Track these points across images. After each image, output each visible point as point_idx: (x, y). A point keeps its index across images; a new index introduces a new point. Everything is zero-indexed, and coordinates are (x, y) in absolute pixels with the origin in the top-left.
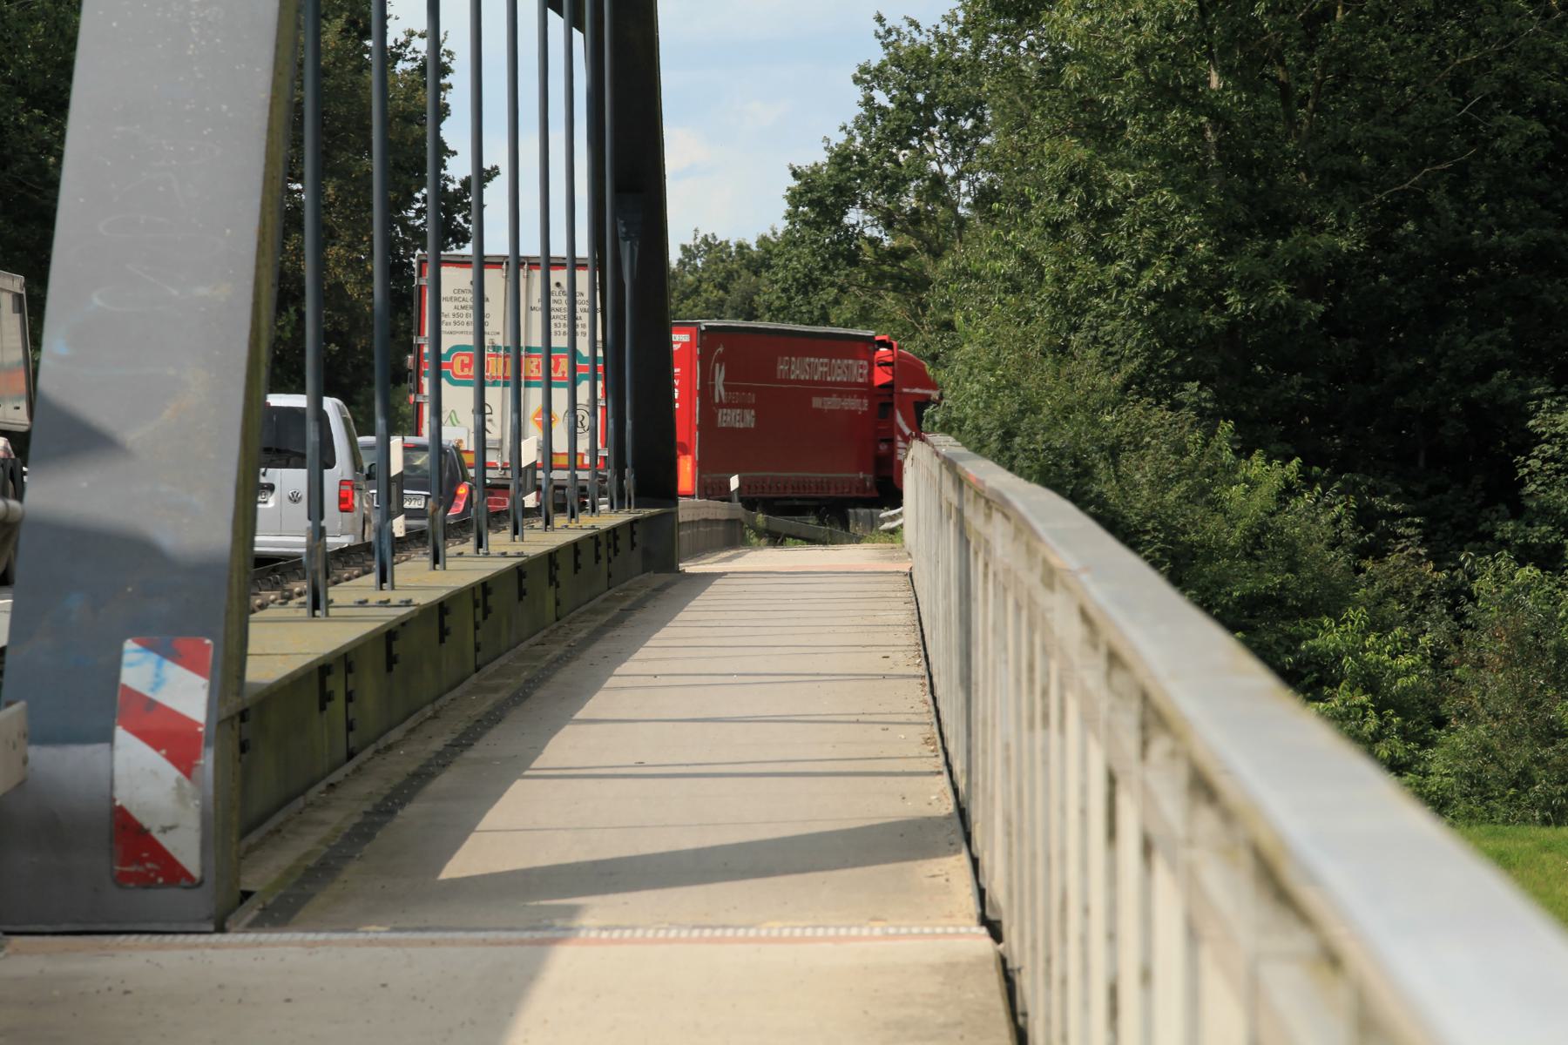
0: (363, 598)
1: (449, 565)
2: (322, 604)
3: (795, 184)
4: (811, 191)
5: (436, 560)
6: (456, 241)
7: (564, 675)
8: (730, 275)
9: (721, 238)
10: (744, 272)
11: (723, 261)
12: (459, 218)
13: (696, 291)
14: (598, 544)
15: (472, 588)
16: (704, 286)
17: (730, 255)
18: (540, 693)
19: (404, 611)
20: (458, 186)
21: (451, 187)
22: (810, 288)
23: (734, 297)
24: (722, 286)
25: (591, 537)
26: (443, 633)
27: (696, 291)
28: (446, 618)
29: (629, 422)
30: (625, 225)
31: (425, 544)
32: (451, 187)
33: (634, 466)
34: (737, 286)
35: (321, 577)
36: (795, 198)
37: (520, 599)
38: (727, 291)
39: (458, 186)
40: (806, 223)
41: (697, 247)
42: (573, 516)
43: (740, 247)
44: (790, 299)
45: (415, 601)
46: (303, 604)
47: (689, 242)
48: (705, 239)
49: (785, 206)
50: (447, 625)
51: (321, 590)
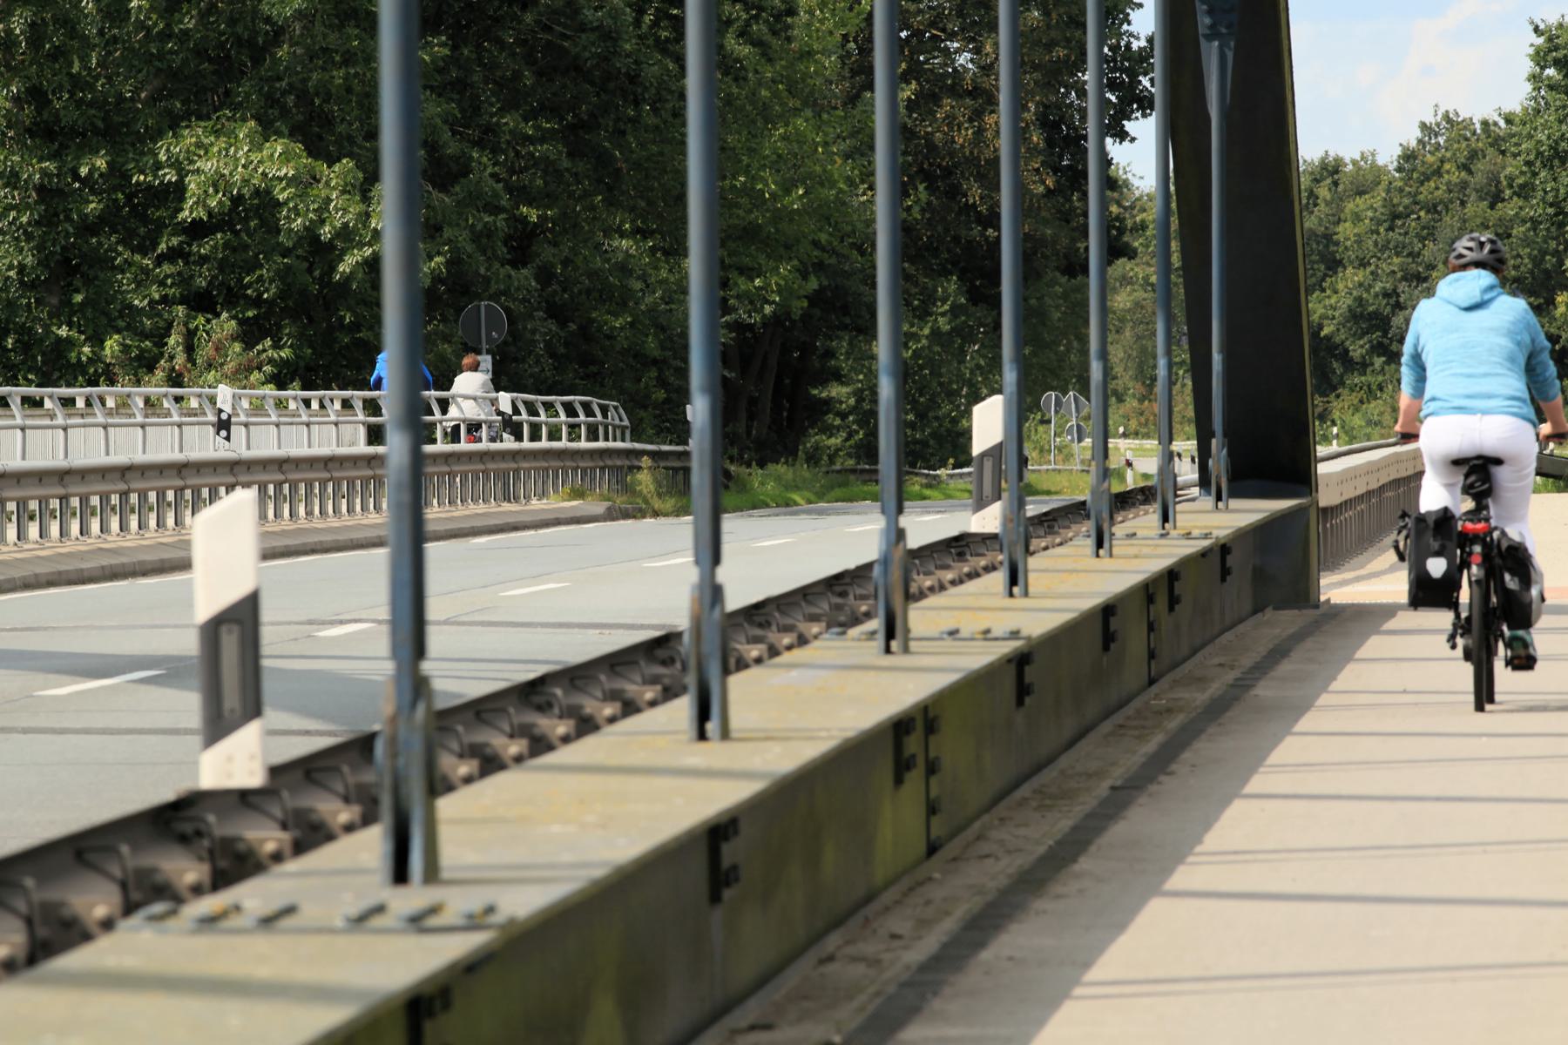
0: (951, 626)
1: (1115, 551)
2: (1106, 545)
3: (1540, 41)
4: (1556, 49)
5: (1100, 544)
6: (1142, 108)
7: (1137, 822)
8: (1474, 155)
9: (1464, 114)
10: (1490, 151)
11: (1467, 139)
12: (1145, 82)
13: (1438, 173)
14: (1150, 599)
15: (1085, 619)
16: (1447, 166)
17: (1474, 133)
18: (1084, 864)
19: (1206, 543)
20: (1143, 43)
21: (1135, 45)
22: (1556, 162)
23: (1478, 179)
24: (1465, 167)
25: (1204, 554)
26: (1225, 572)
27: (1438, 173)
28: (1176, 584)
29: (1217, 358)
30: (1210, 12)
31: (1088, 517)
32: (1135, 45)
33: (1225, 435)
34: (1480, 166)
35: (1020, 550)
36: (1540, 58)
37: (1020, 702)
38: (1470, 172)
39: (1143, 43)
40: (1551, 88)
41: (1438, 125)
42: (1219, 498)
43: (1485, 123)
44: (1535, 174)
45: (1025, 632)
46: (872, 634)
47: (1430, 119)
48: (1446, 117)
49: (1528, 66)
50: (1177, 592)
51: (1106, 526)
